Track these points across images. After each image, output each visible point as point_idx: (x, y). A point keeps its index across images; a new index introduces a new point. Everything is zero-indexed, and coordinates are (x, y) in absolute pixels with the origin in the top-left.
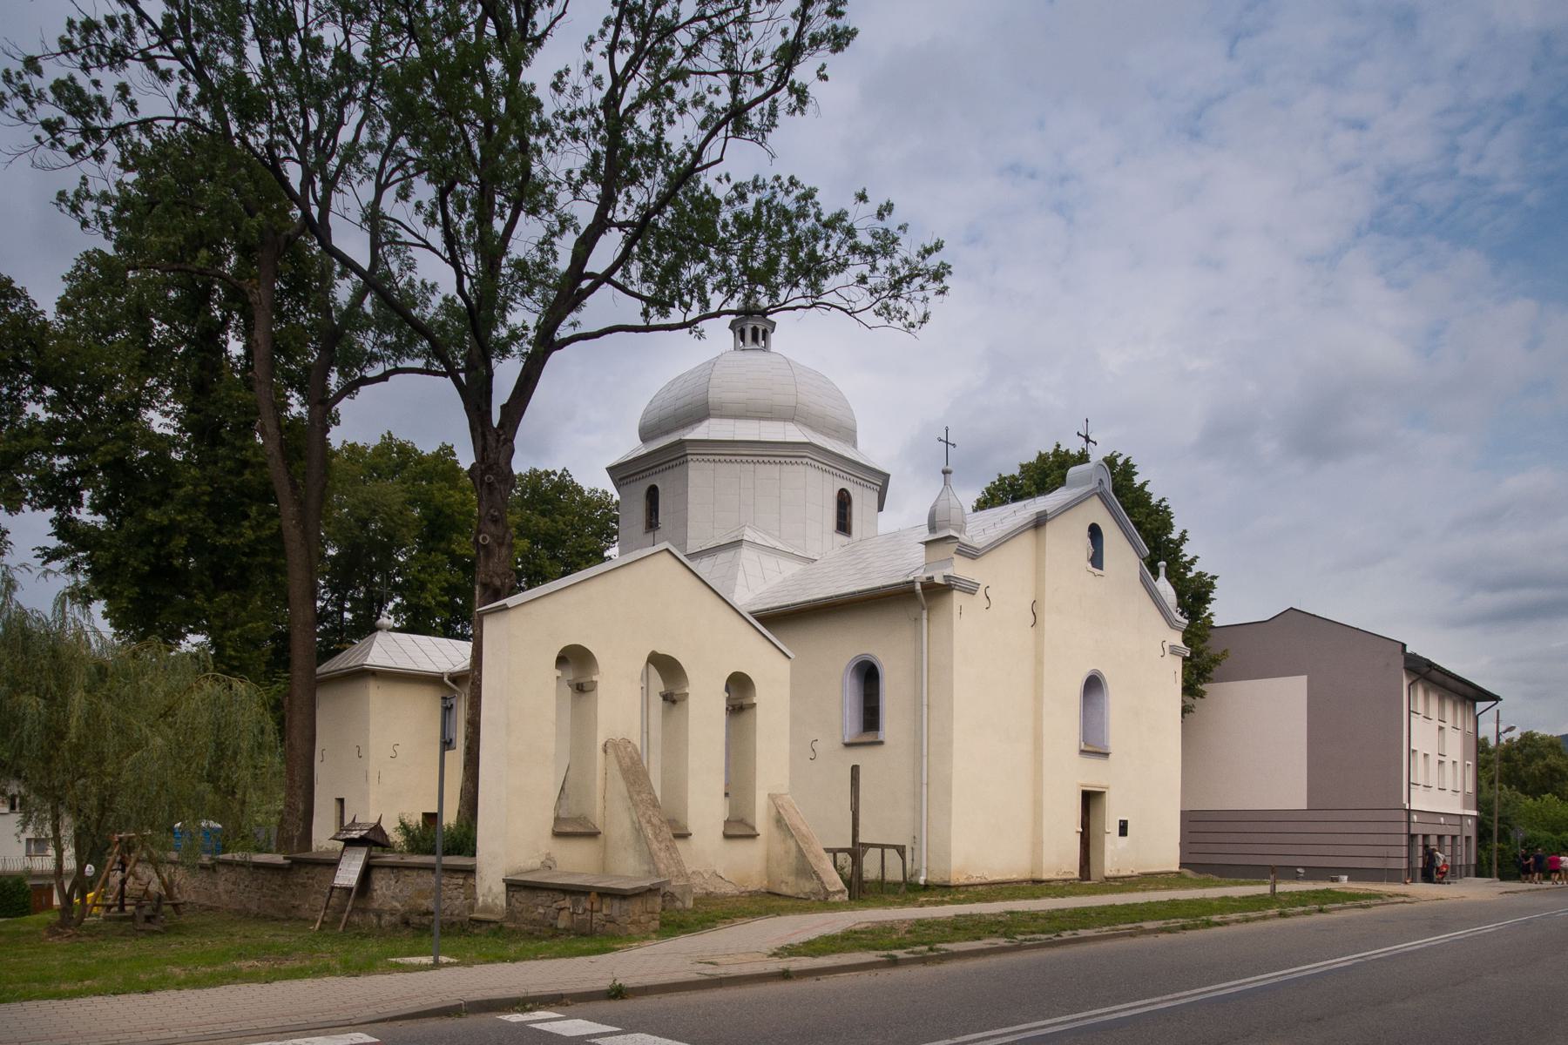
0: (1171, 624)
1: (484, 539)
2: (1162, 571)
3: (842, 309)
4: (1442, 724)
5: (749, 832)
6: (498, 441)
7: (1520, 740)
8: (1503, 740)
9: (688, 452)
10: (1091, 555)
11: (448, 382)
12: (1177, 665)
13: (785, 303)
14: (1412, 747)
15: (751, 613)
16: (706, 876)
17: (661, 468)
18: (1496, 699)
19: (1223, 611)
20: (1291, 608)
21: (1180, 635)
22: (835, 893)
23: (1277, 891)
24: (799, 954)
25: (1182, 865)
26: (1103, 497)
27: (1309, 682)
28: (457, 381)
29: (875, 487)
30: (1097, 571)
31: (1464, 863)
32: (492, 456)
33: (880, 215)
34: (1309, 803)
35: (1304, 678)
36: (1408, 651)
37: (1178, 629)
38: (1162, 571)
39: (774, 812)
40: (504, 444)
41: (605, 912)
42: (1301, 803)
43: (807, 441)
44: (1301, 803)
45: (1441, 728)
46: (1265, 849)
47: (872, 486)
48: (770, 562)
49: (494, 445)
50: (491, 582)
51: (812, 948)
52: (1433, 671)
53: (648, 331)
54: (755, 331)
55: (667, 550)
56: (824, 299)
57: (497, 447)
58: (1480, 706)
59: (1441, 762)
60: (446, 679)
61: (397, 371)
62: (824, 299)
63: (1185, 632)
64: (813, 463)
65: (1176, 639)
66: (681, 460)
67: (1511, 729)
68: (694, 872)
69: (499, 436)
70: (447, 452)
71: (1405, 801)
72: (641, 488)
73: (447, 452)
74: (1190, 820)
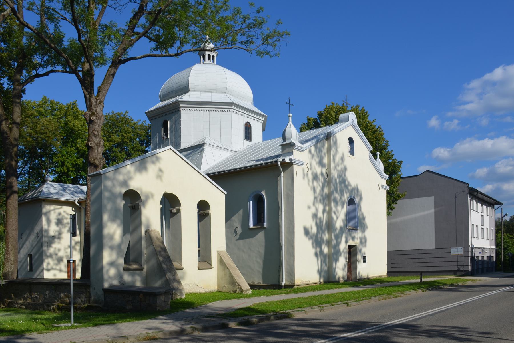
0: (382, 178)
1: (91, 144)
2: (378, 156)
3: (244, 49)
4: (483, 214)
5: (210, 267)
6: (96, 102)
7: (510, 220)
8: (504, 219)
9: (181, 106)
10: (349, 150)
11: (74, 76)
12: (385, 192)
14: (472, 223)
15: (207, 175)
16: (191, 285)
17: (169, 113)
18: (501, 204)
19: (405, 171)
20: (428, 170)
21: (385, 181)
22: (246, 291)
23: (423, 281)
24: (338, 327)
25: (388, 272)
26: (353, 126)
27: (435, 199)
28: (78, 76)
29: (261, 121)
30: (352, 156)
31: (491, 266)
32: (94, 108)
33: (258, 12)
34: (435, 247)
35: (433, 197)
36: (470, 186)
37: (384, 179)
38: (378, 156)
39: (219, 258)
40: (100, 103)
42: (431, 245)
43: (232, 102)
44: (431, 245)
45: (482, 216)
46: (406, 265)
47: (260, 120)
48: (217, 152)
49: (95, 104)
50: (95, 162)
51: (450, 330)
52: (479, 194)
53: (162, 57)
54: (209, 56)
55: (171, 149)
56: (237, 45)
57: (96, 105)
58: (496, 206)
59: (482, 228)
60: (76, 203)
61: (38, 76)
62: (237, 45)
63: (387, 180)
64: (235, 111)
65: (384, 183)
66: (176, 110)
67: (506, 215)
68: (186, 284)
69: (97, 100)
70: (73, 105)
71: (470, 244)
72: (161, 121)
73: (73, 105)
74: (390, 254)
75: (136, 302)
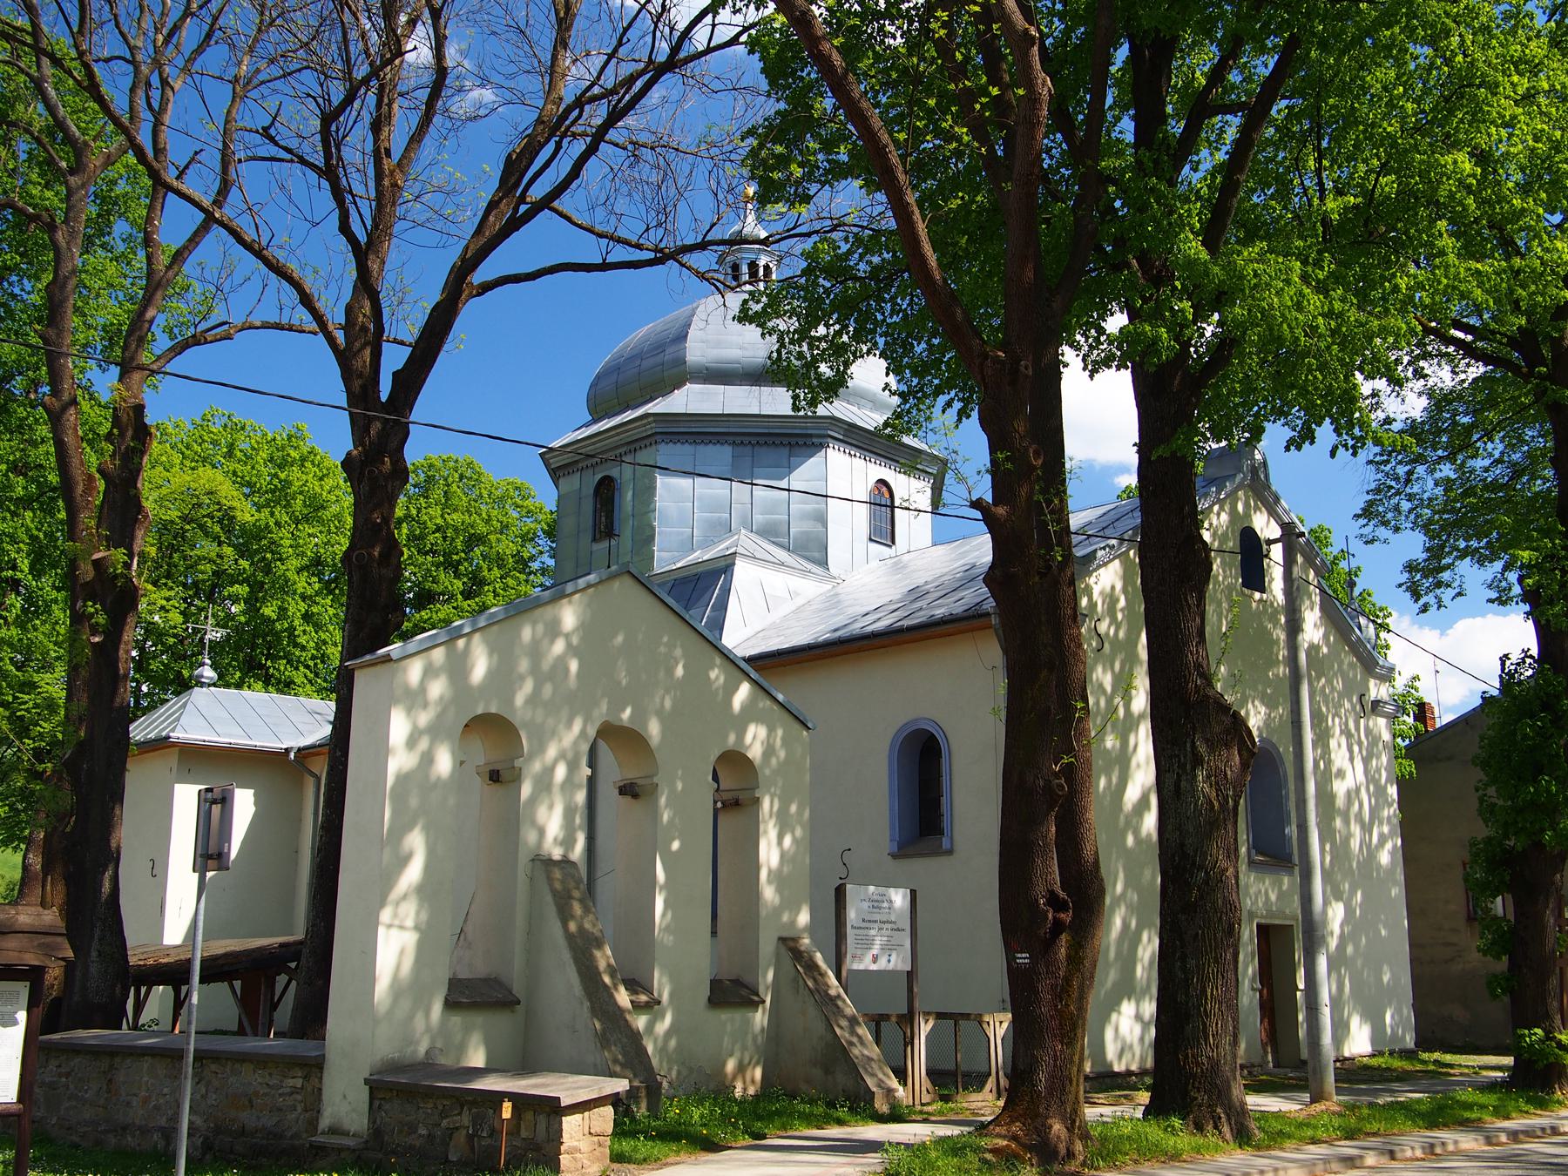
13: (794, 228)
41: (524, 1134)
75: (485, 1134)
